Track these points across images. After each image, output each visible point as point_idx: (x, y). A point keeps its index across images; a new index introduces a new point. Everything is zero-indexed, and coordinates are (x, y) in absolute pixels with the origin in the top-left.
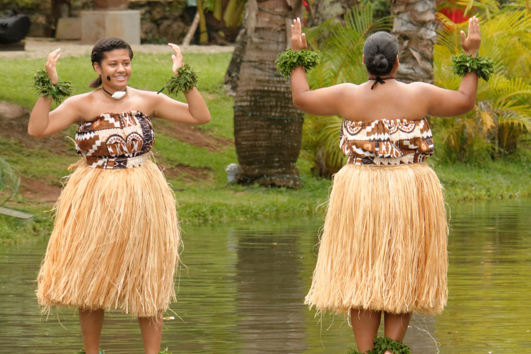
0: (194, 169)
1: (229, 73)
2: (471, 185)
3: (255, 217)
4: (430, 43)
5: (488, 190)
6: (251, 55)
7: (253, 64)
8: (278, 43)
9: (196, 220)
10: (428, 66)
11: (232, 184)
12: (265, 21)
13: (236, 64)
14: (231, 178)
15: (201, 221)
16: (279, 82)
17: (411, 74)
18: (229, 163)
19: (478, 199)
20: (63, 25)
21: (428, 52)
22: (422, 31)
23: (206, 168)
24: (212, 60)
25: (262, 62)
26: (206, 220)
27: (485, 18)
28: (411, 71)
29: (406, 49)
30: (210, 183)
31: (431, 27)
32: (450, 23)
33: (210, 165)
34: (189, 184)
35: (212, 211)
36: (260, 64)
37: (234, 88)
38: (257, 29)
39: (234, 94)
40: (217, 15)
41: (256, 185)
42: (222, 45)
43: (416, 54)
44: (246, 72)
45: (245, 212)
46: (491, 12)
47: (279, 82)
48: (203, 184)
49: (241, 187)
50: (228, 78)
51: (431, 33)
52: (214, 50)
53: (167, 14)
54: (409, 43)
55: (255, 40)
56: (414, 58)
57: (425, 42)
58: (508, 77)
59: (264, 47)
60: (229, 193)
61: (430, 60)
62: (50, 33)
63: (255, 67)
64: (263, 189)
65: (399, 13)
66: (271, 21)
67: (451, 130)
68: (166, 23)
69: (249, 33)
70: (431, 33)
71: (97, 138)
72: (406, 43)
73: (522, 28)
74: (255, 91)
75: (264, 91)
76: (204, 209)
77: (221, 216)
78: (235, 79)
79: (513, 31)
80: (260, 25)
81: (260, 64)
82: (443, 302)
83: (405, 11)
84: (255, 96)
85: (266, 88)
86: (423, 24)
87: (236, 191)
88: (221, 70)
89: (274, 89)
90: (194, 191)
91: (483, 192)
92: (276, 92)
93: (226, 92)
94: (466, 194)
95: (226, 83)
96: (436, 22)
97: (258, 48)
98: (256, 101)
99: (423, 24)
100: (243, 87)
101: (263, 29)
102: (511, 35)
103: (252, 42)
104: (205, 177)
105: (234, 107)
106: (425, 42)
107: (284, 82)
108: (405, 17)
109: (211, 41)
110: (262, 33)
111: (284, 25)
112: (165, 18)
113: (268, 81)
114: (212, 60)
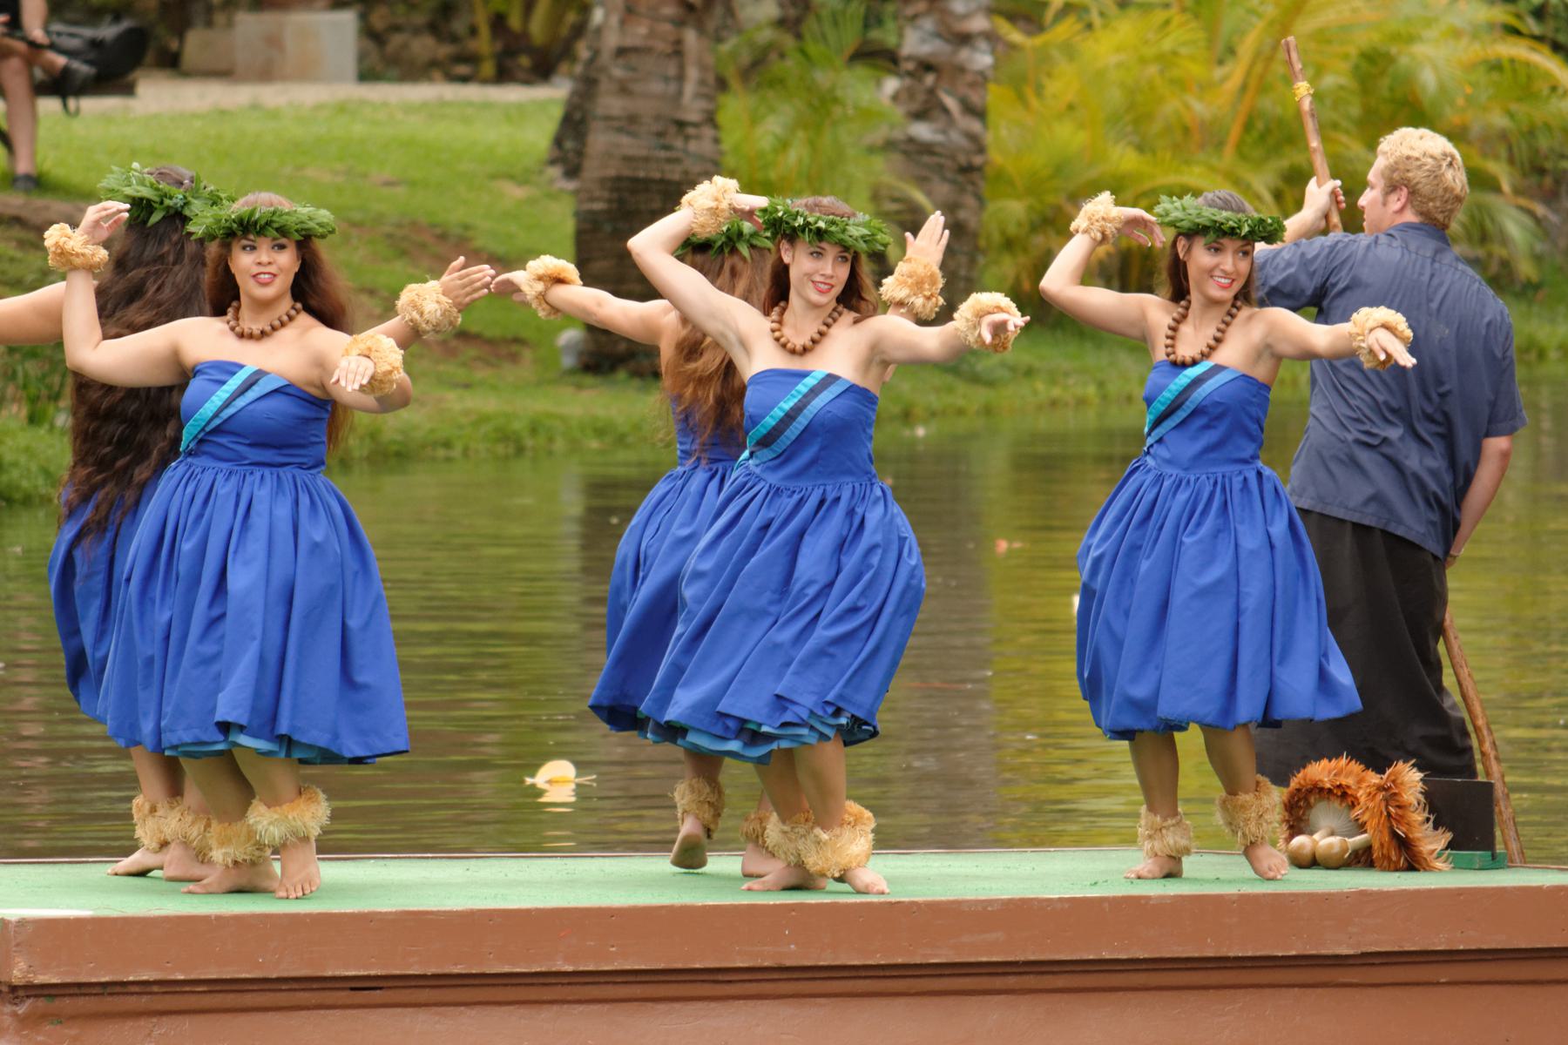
0: (491, 342)
1: (558, 141)
2: (1067, 374)
3: (621, 440)
4: (979, 79)
5: (1101, 385)
6: (610, 103)
7: (616, 124)
8: (666, 79)
9: (500, 449)
10: (975, 126)
11: (571, 372)
12: (639, 32)
13: (574, 125)
14: (568, 361)
15: (511, 450)
16: (669, 161)
17: (940, 144)
18: (561, 329)
19: (1082, 402)
20: (195, 44)
21: (975, 98)
22: (964, 54)
23: (517, 340)
24: (515, 114)
25: (633, 119)
26: (520, 450)
27: (1089, 26)
28: (939, 138)
29: (931, 92)
30: (526, 369)
31: (983, 45)
32: (1016, 36)
33: (525, 333)
34: (481, 374)
35: (534, 430)
36: (630, 123)
37: (572, 172)
38: (621, 52)
39: (571, 185)
40: (515, 22)
41: (622, 375)
42: (527, 82)
43: (950, 102)
44: (599, 140)
45: (600, 432)
46: (1102, 14)
47: (669, 161)
48: (510, 373)
49: (589, 380)
50: (557, 153)
51: (982, 59)
52: (512, 94)
53: (400, 20)
54: (938, 79)
55: (618, 72)
56: (946, 111)
57: (969, 78)
58: (1140, 148)
59: (637, 87)
60: (567, 392)
61: (979, 113)
62: (171, 63)
63: (620, 130)
64: (636, 382)
65: (915, 17)
66: (652, 34)
67: (1022, 259)
68: (396, 40)
69: (606, 57)
70: (982, 59)
71: (1386, 403)
72: (930, 79)
73: (1167, 45)
74: (618, 179)
75: (635, 180)
76: (518, 426)
77: (551, 440)
78: (571, 155)
79: (1149, 52)
80: (629, 42)
81: (630, 123)
82: (1342, 673)
83: (929, 12)
84: (617, 190)
85: (642, 174)
86: (965, 39)
87: (579, 387)
88: (539, 135)
89: (657, 175)
90: (494, 388)
91: (1091, 390)
92: (662, 181)
93: (552, 181)
94: (1056, 392)
95: (553, 162)
96: (991, 37)
97: (624, 90)
98: (621, 201)
99: (965, 39)
100: (593, 170)
101: (635, 50)
102: (1143, 61)
103: (610, 78)
104: (514, 358)
105: (577, 214)
106: (969, 78)
107: (677, 161)
108: (928, 24)
109: (503, 76)
110: (634, 59)
111: (679, 42)
112: (396, 28)
113: (646, 159)
114: (515, 114)
